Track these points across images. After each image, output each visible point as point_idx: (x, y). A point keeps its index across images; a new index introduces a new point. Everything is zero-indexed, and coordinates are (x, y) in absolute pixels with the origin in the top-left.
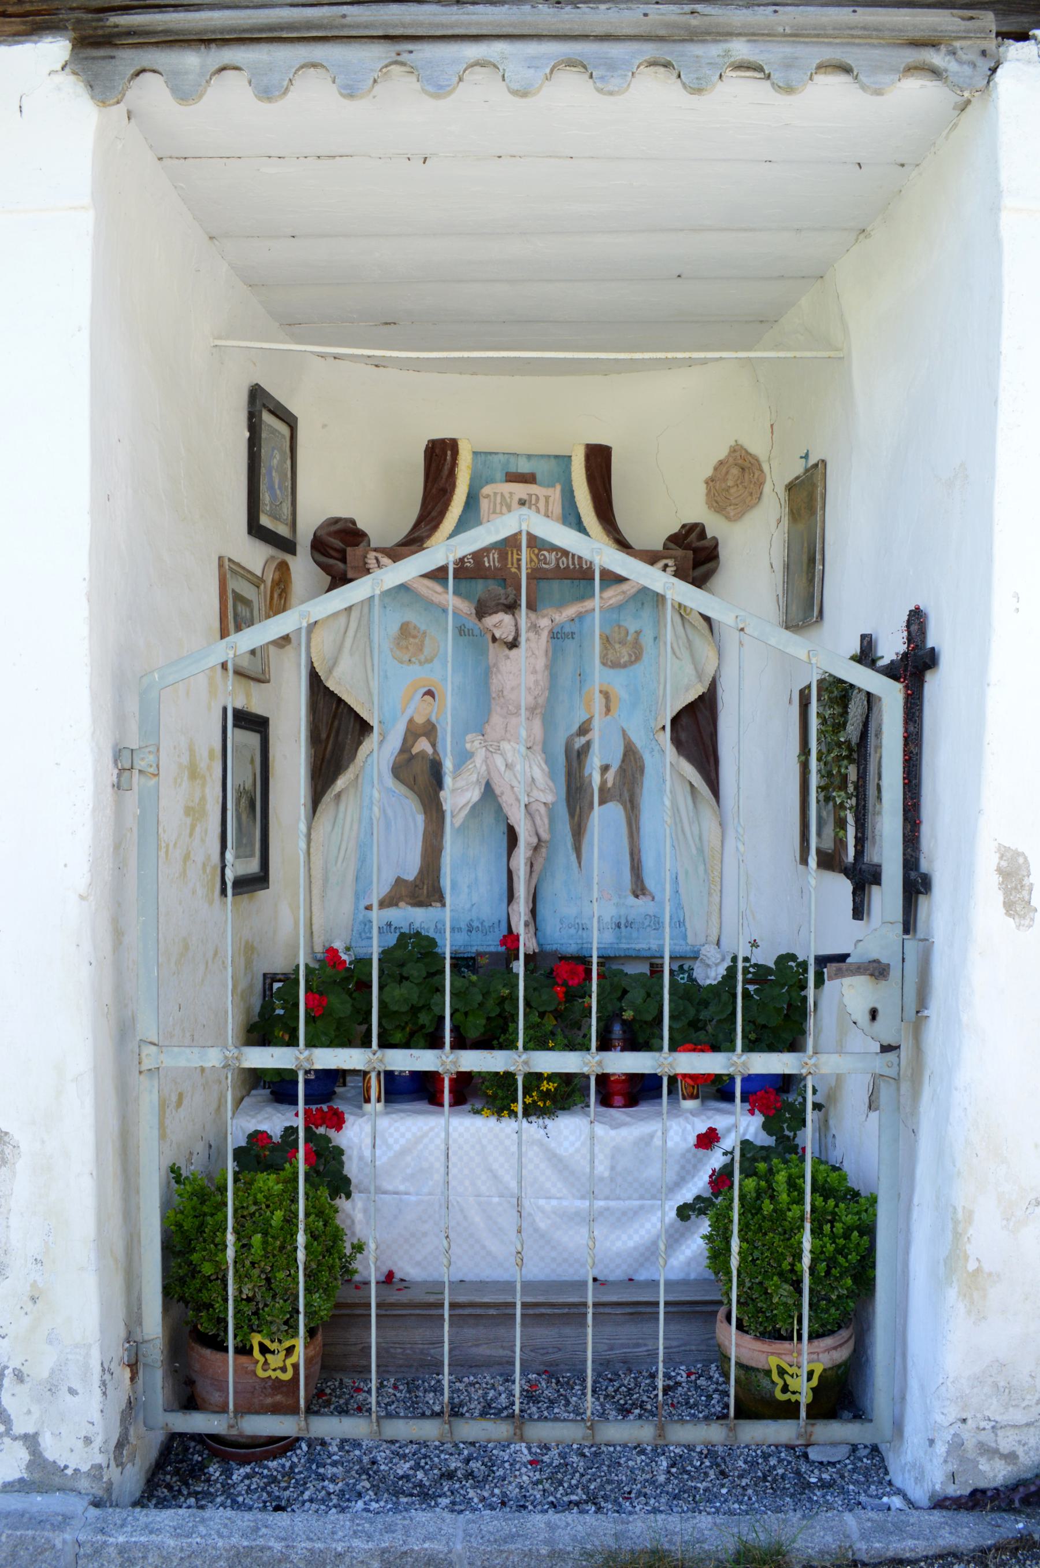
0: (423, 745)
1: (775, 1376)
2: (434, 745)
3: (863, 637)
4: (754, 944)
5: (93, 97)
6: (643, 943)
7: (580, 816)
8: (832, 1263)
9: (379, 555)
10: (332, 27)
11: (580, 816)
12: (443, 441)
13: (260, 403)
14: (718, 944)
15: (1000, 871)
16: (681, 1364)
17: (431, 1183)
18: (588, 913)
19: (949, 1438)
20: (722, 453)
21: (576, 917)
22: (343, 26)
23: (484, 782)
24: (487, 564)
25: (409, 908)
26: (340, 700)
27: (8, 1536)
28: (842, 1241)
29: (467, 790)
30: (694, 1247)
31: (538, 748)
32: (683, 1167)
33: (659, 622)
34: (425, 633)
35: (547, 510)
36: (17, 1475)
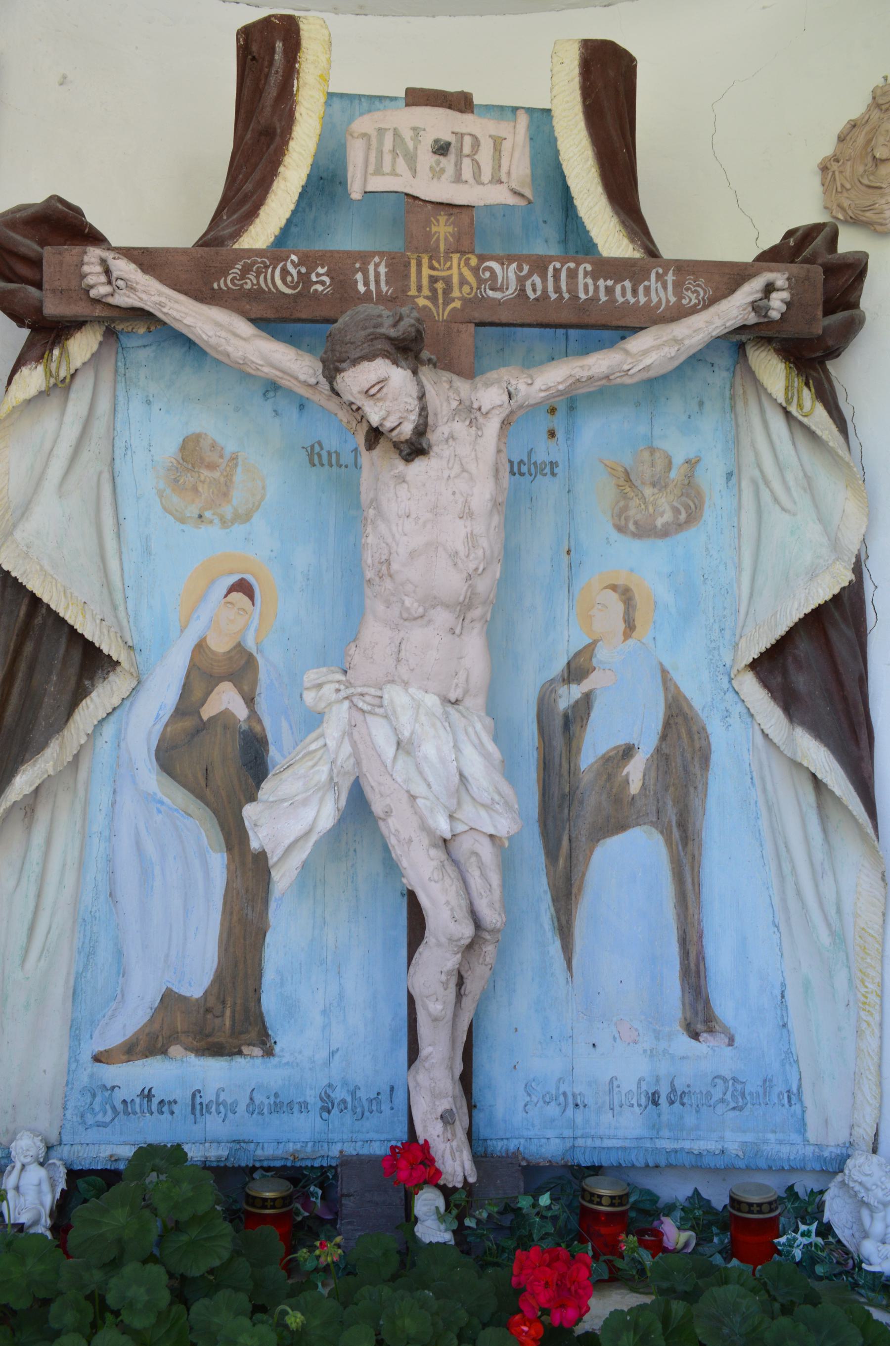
0: (226, 700)
2: (250, 701)
7: (570, 856)
11: (570, 856)
21: (561, 1080)
23: (345, 785)
24: (361, 288)
25: (192, 1058)
26: (35, 601)
29: (305, 802)
31: (475, 703)
33: (737, 441)
34: (234, 458)
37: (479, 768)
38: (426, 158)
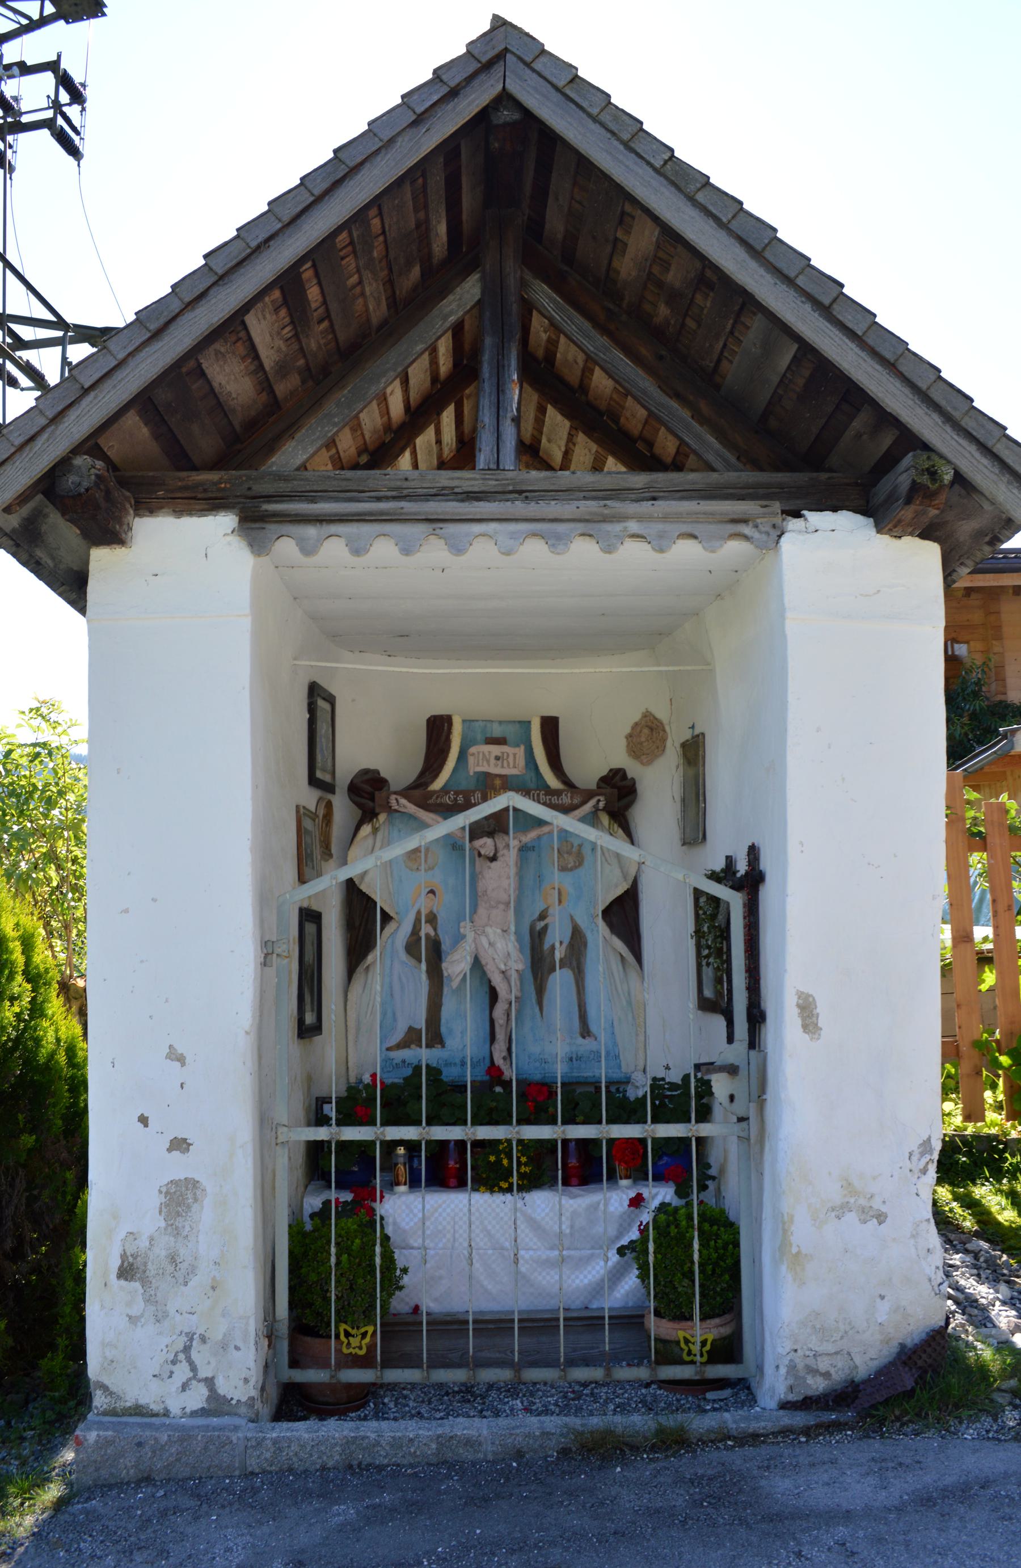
1: (683, 1345)
2: (435, 929)
3: (727, 857)
4: (668, 1068)
5: (252, 552)
6: (587, 1073)
7: (541, 979)
8: (716, 1264)
9: (399, 797)
10: (395, 514)
11: (541, 979)
12: (441, 717)
13: (314, 691)
14: (644, 1071)
15: (798, 1006)
16: (623, 1360)
17: (444, 1240)
18: (548, 1047)
19: (787, 1363)
20: (637, 717)
22: (402, 514)
27: (203, 1436)
28: (722, 1251)
30: (631, 1283)
32: (621, 1225)
35: (515, 762)
36: (200, 1406)
37: (515, 954)
38: (493, 761)
